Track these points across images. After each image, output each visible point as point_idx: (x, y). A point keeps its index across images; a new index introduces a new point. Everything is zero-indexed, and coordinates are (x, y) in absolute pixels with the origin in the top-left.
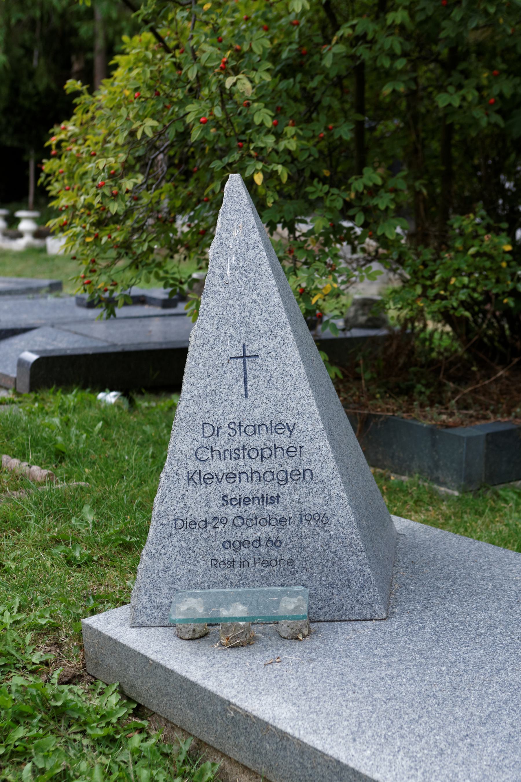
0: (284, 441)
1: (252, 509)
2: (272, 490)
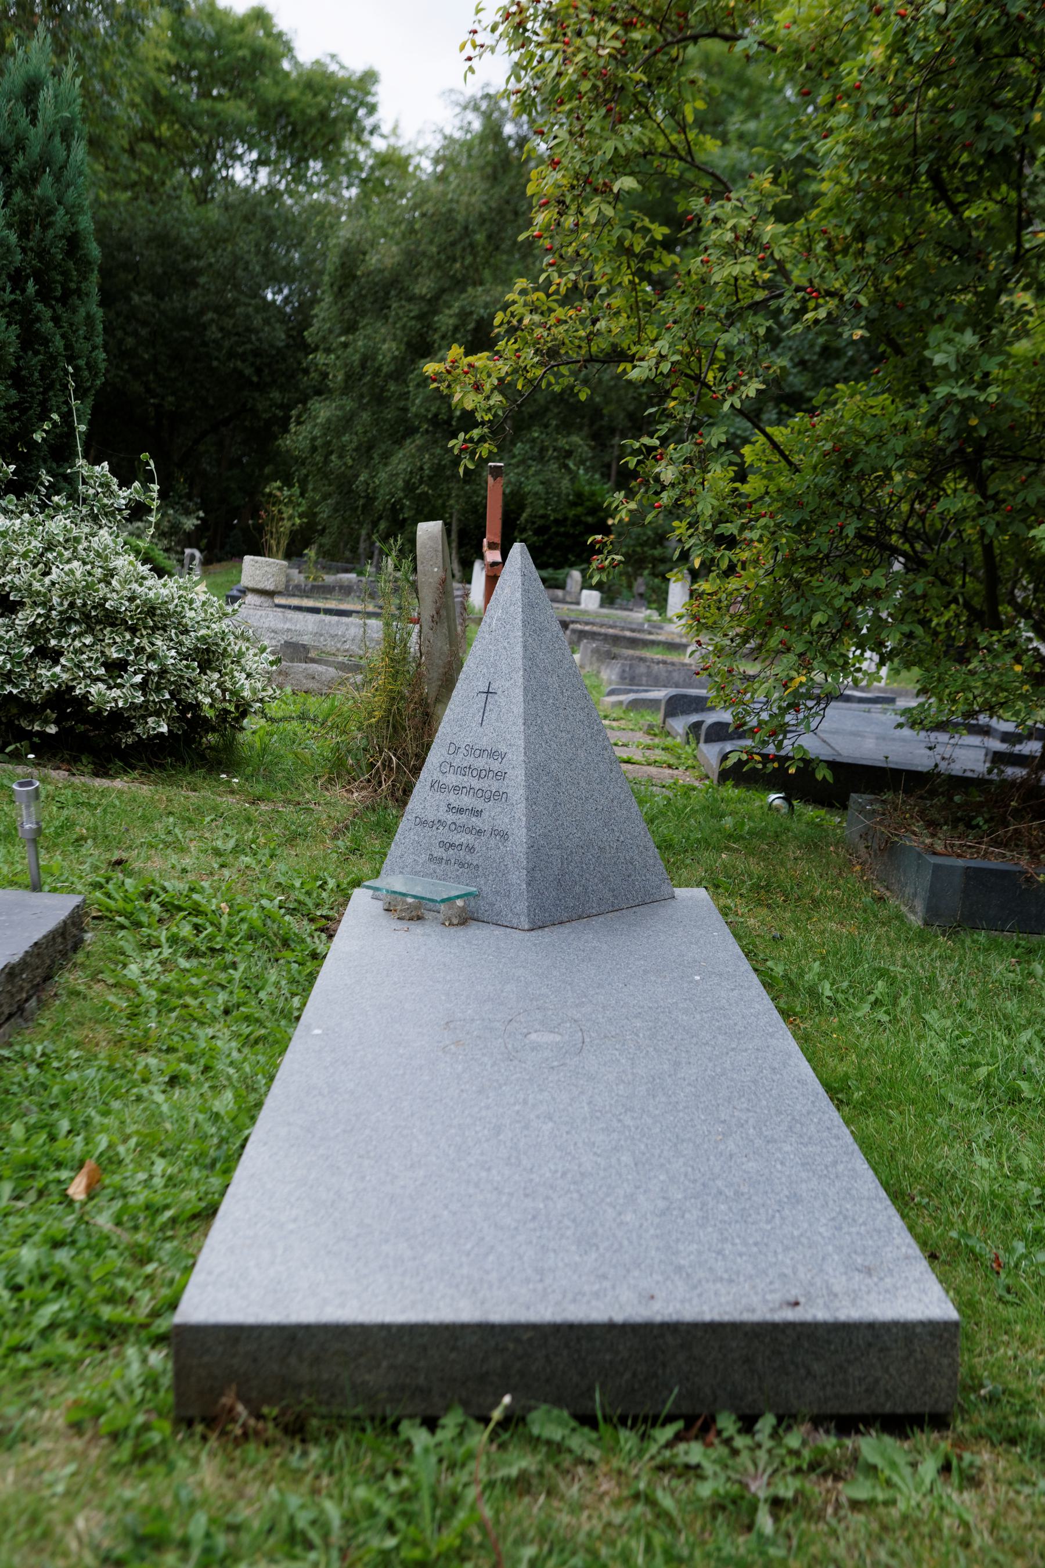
0: (495, 766)
1: (462, 819)
2: (479, 804)
